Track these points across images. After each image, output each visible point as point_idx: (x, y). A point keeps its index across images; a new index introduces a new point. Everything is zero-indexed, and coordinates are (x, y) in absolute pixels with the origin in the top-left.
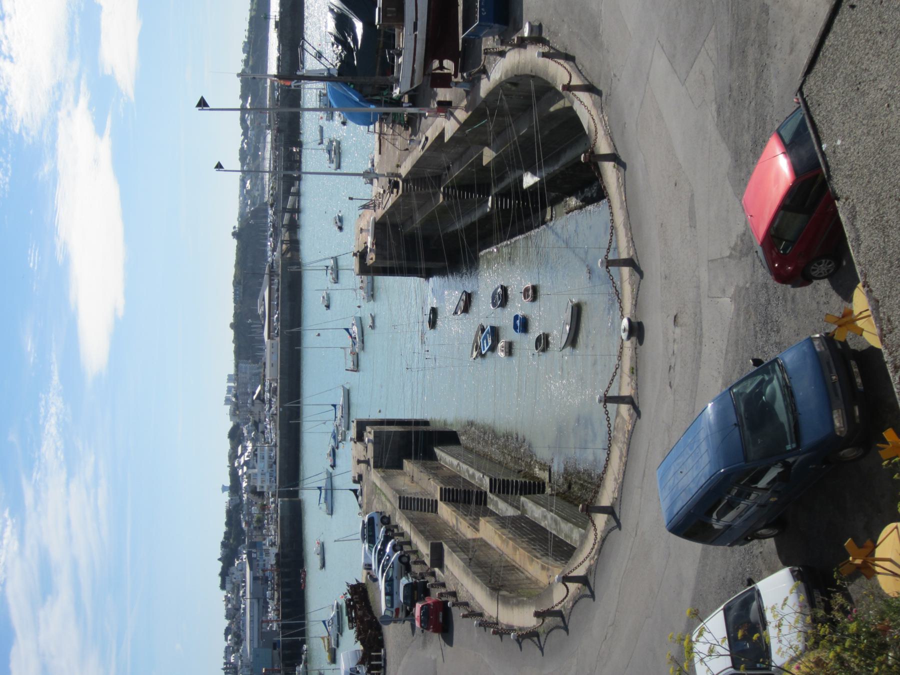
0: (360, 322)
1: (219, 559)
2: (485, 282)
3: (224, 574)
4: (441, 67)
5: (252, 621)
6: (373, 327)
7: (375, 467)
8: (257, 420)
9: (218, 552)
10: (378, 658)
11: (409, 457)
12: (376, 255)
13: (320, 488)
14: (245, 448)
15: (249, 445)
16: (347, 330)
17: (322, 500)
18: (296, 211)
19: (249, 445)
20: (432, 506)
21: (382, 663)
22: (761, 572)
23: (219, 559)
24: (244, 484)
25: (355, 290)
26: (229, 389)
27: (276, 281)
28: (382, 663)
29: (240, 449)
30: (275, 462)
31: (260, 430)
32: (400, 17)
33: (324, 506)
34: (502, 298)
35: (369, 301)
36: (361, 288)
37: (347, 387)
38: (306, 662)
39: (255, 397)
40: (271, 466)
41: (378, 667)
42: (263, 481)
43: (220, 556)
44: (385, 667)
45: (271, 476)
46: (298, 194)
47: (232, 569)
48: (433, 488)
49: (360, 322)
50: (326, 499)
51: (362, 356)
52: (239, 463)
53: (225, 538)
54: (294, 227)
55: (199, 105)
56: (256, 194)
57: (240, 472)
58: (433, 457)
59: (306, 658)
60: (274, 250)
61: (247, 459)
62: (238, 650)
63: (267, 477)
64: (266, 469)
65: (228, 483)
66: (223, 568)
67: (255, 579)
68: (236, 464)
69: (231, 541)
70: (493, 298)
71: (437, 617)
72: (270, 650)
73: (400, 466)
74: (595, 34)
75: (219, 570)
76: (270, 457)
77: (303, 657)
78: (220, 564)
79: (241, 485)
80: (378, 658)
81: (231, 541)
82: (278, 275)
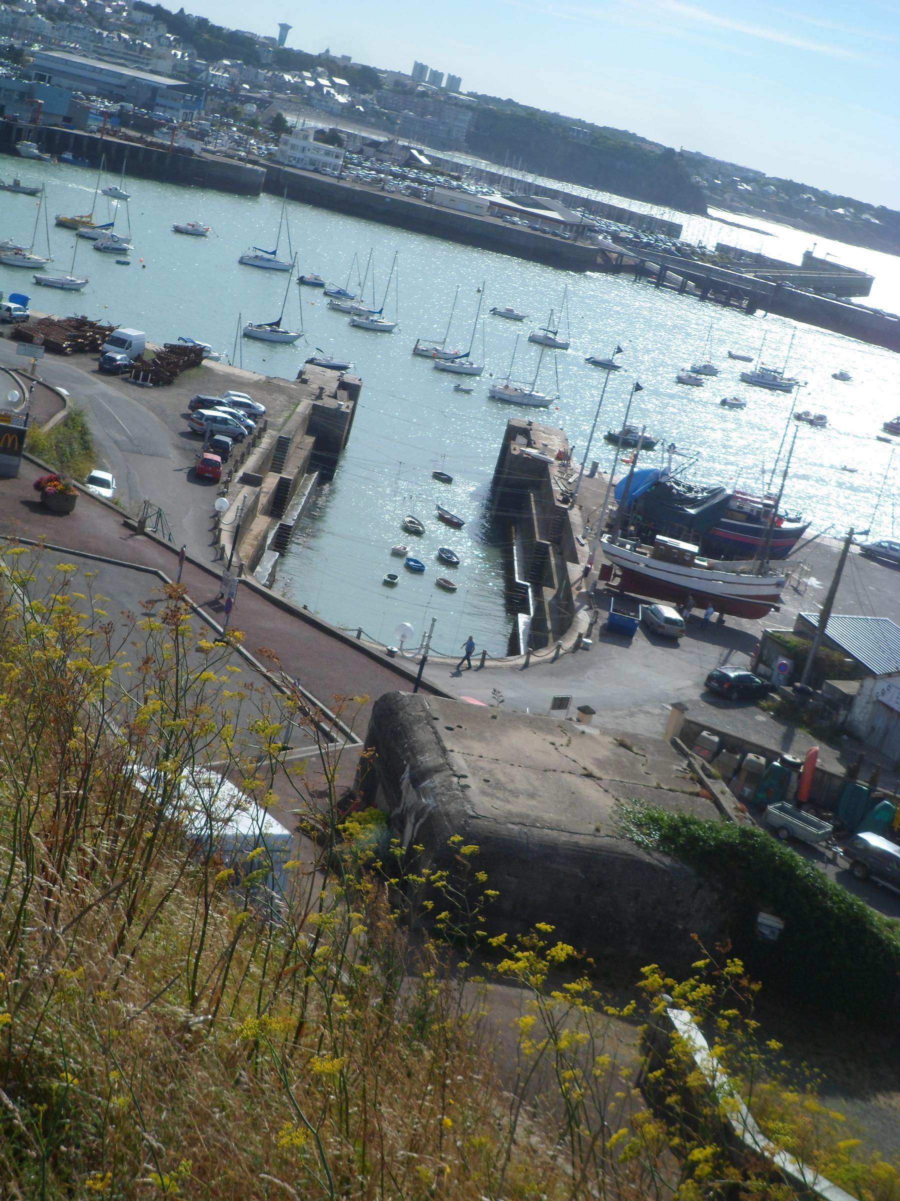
0: (473, 373)
1: (182, 10)
2: (467, 547)
3: (159, 13)
4: (616, 575)
5: (94, 69)
6: (457, 389)
7: (315, 407)
8: (381, 148)
9: (194, 10)
10: (145, 379)
11: (317, 446)
12: (516, 456)
13: (274, 253)
14: (341, 89)
15: (342, 99)
16: (467, 355)
17: (259, 253)
18: (660, 281)
19: (342, 99)
20: (278, 470)
21: (140, 382)
22: (130, 741)
23: (182, 10)
24: (287, 77)
25: (507, 379)
26: (437, 76)
27: (568, 234)
28: (140, 382)
29: (344, 82)
30: (316, 171)
31: (366, 149)
32: (657, 556)
33: (252, 254)
34: (447, 559)
35: (491, 391)
36: (507, 387)
37: (395, 330)
38: (39, 158)
39: (415, 152)
40: (312, 162)
41: (136, 377)
42: (293, 147)
43: (187, 12)
44: (134, 384)
45: (299, 160)
46: (682, 290)
47: (162, 28)
48: (290, 472)
49: (473, 373)
50: (262, 258)
51: (430, 364)
52: (320, 75)
53: (213, 26)
54: (639, 272)
55: (638, 384)
56: (727, 196)
57: (307, 74)
58: (310, 472)
59: (44, 160)
60: (616, 238)
61: (325, 90)
62: (40, 11)
63: (299, 154)
64: (310, 155)
65: (292, 43)
66: (168, 13)
67: (155, 89)
68: (320, 69)
69: (206, 36)
70: (449, 551)
71: (209, 472)
72: (65, 114)
73: (309, 431)
74: (552, 674)
75: (166, 6)
76: (325, 164)
77: (46, 156)
78: (175, 11)
79: (288, 71)
80: (145, 379)
81: (206, 36)
82: (575, 240)
